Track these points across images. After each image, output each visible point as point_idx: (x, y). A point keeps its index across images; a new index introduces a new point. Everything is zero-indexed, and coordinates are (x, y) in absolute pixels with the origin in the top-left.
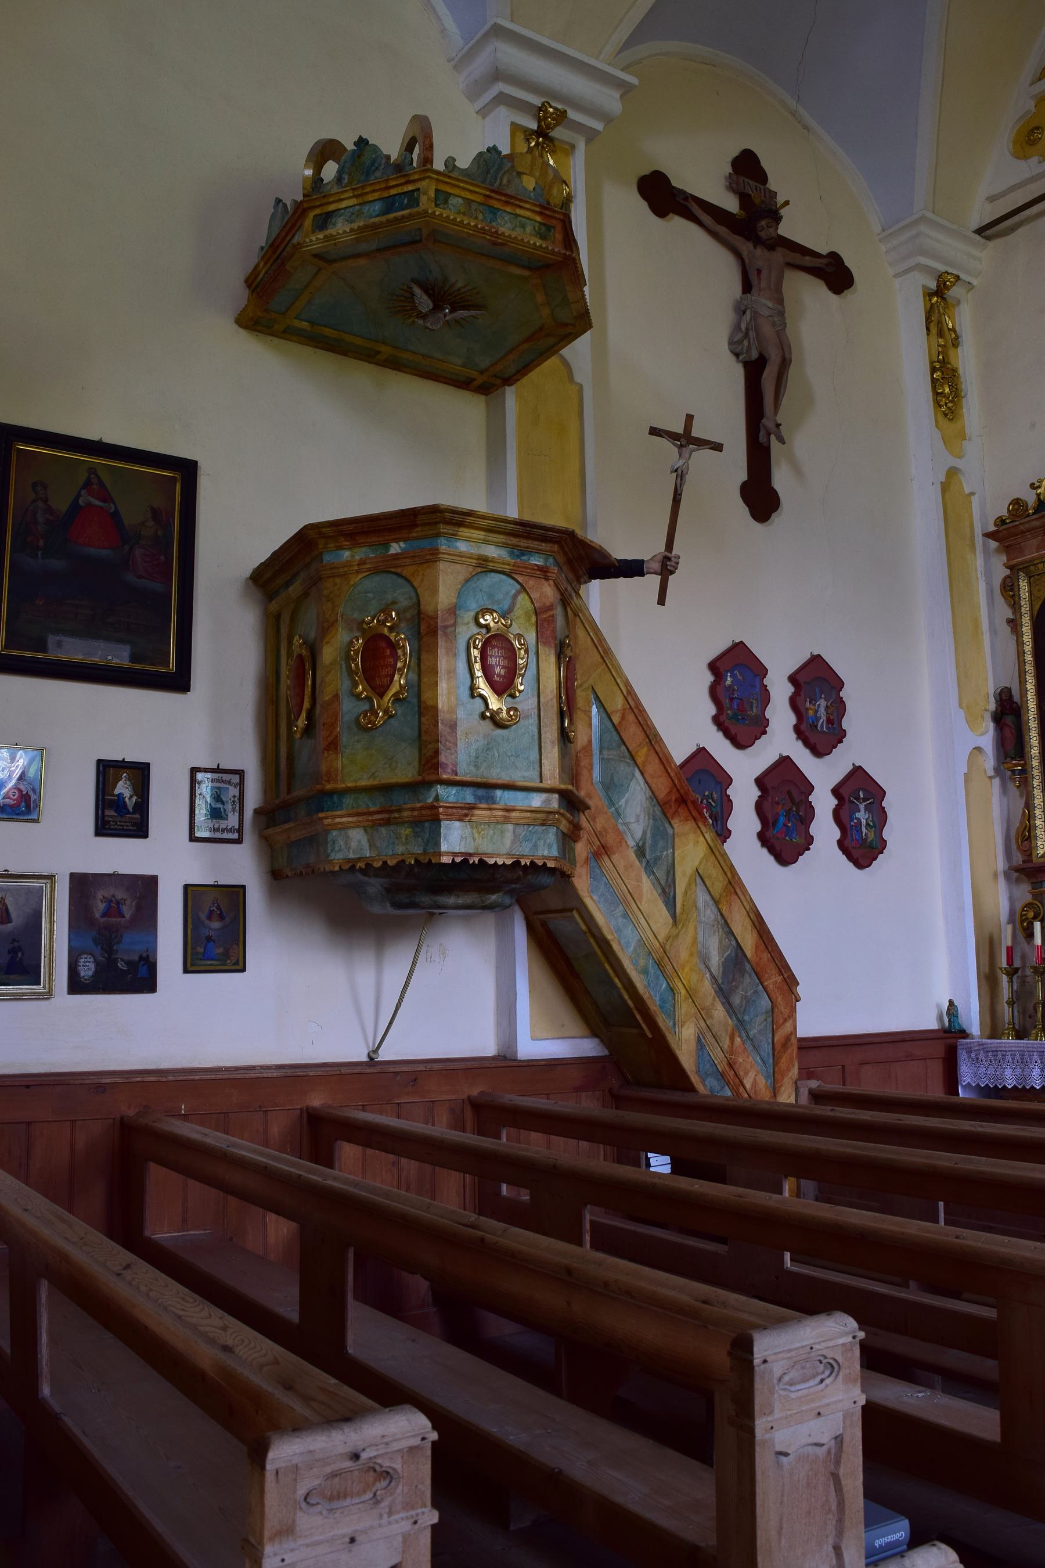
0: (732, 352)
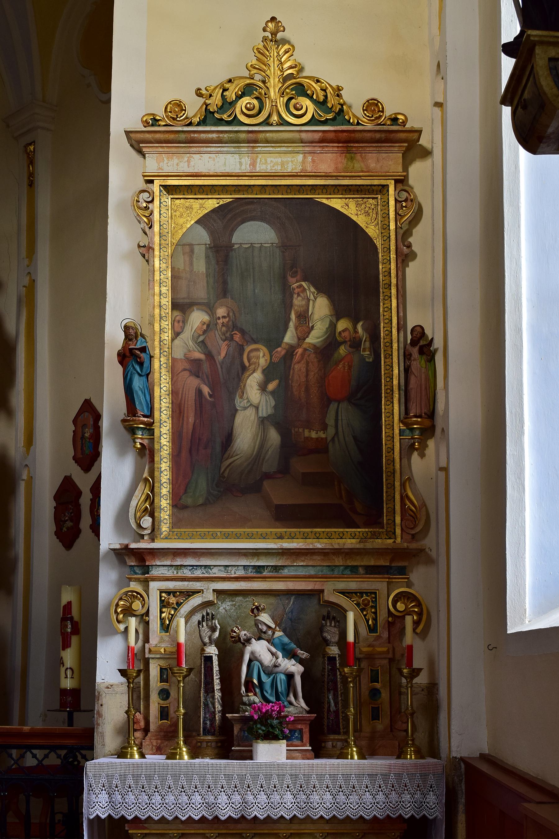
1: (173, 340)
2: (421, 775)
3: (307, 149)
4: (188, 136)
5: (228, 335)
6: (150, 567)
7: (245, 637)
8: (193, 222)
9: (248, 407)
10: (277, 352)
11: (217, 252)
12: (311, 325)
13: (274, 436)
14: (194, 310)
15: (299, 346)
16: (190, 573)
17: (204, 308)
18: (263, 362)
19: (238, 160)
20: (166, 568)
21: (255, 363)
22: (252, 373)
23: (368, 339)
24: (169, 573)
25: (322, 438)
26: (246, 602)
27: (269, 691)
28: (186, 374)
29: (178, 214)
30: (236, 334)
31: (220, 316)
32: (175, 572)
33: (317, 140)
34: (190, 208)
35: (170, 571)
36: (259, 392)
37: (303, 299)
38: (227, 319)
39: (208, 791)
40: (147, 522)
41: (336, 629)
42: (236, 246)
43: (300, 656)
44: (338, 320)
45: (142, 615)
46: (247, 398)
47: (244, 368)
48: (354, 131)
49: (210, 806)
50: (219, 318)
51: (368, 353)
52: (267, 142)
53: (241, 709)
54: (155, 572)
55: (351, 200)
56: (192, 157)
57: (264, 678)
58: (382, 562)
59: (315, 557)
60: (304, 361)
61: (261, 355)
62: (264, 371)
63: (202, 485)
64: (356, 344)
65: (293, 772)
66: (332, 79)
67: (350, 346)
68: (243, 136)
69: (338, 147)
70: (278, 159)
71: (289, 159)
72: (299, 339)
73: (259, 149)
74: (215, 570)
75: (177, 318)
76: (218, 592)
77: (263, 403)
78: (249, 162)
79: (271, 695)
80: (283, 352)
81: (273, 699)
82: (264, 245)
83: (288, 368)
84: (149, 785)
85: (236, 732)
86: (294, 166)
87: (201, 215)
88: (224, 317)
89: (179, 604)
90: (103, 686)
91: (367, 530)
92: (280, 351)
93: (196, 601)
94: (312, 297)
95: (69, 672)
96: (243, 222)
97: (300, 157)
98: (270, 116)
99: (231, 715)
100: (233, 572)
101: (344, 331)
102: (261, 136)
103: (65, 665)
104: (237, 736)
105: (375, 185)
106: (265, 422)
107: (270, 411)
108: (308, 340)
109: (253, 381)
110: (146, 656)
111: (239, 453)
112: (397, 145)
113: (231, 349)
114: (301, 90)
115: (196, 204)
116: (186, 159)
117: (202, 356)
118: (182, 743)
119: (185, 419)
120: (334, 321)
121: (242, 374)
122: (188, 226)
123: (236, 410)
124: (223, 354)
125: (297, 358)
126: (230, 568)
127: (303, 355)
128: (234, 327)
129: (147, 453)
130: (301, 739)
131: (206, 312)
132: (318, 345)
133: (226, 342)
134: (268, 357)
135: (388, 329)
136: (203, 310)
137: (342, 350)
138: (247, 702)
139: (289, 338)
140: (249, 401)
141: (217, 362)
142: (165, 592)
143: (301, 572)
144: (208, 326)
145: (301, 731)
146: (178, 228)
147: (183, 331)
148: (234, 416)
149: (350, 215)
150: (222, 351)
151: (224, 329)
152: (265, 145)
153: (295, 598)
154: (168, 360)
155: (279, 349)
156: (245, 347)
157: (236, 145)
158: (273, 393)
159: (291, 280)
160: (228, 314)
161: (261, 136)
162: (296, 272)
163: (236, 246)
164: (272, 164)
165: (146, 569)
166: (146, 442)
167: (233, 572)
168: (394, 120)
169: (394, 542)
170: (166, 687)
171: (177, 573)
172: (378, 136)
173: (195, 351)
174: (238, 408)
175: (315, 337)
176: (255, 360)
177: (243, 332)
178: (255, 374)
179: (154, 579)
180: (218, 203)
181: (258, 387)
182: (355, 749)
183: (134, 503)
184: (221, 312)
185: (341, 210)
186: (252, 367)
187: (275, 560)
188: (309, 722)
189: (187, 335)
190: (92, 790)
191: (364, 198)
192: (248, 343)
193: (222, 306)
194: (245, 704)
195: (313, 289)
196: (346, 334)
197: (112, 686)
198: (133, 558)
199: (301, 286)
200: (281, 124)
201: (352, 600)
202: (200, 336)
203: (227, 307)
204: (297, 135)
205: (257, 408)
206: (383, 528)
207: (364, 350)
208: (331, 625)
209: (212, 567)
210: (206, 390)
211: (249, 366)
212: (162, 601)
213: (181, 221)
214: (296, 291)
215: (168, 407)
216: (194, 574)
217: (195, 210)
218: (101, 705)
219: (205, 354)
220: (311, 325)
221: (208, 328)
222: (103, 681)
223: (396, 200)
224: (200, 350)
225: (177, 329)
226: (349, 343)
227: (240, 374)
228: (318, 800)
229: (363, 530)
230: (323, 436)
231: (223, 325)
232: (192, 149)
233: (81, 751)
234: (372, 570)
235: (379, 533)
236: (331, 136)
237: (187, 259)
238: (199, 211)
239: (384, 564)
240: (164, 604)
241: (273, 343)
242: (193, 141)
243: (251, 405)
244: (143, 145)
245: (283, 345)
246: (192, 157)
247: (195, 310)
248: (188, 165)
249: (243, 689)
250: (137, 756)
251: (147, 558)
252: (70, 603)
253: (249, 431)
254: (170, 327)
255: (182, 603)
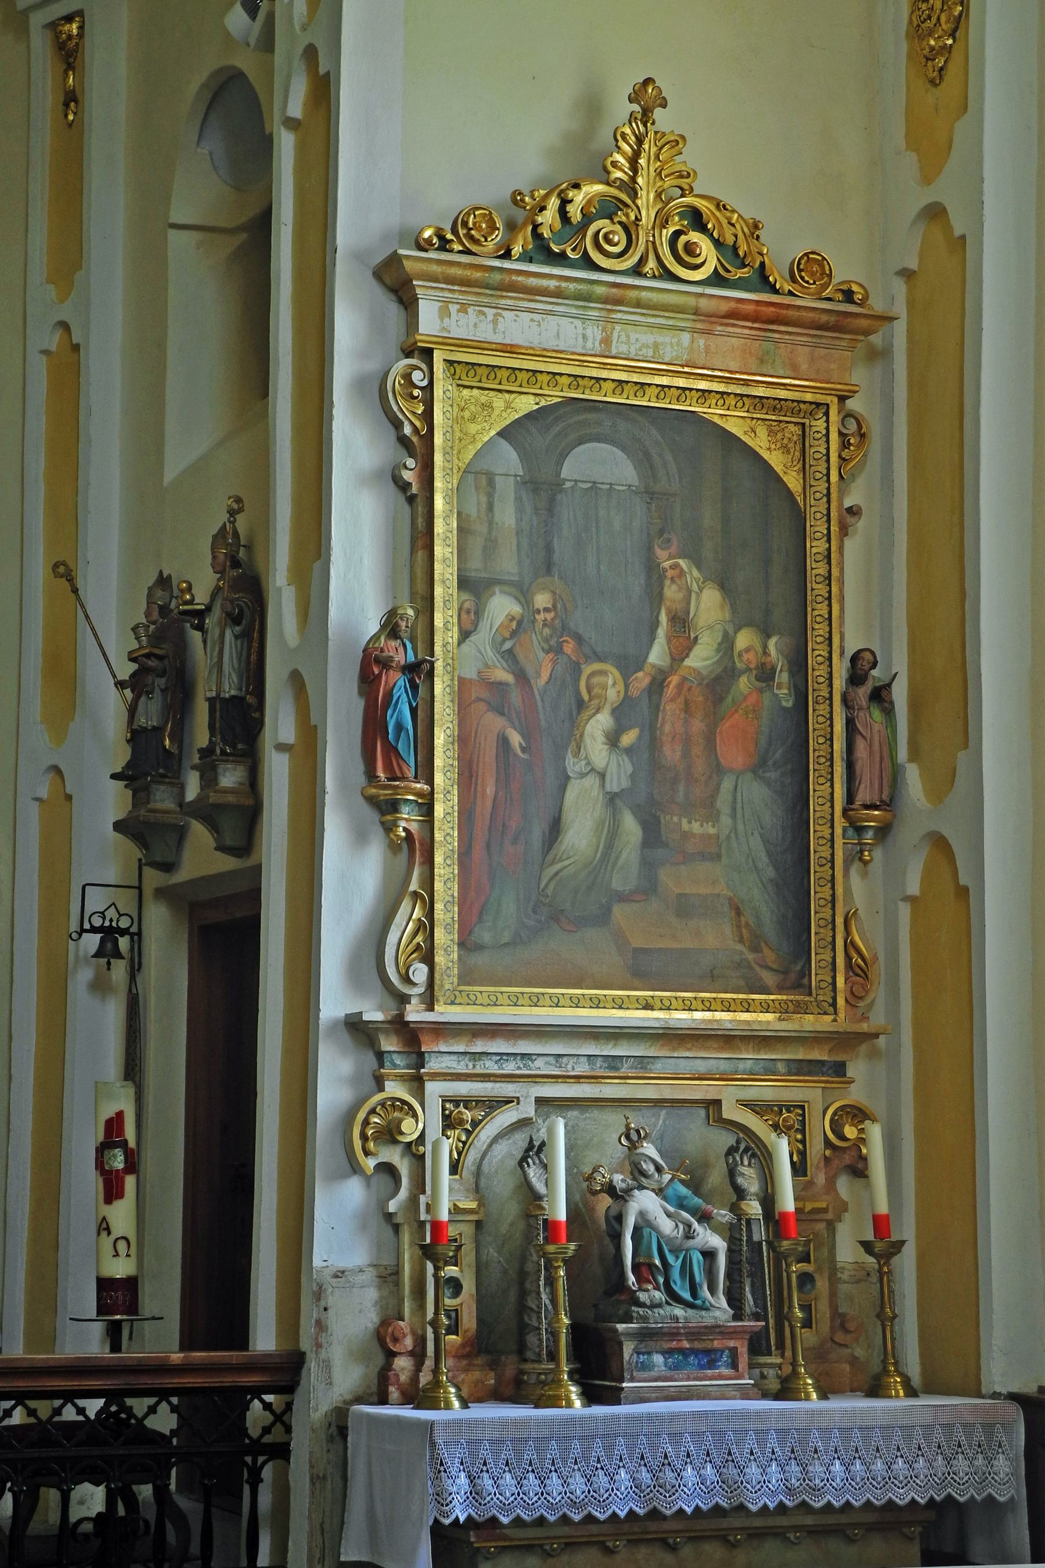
0: (371, 800)
1: (459, 644)
2: (984, 1425)
3: (699, 326)
4: (507, 278)
5: (553, 642)
6: (426, 1055)
7: (624, 1185)
8: (493, 433)
9: (588, 773)
10: (636, 678)
11: (536, 491)
12: (693, 636)
13: (631, 827)
14: (494, 594)
15: (672, 669)
16: (496, 1067)
17: (513, 590)
18: (613, 695)
19: (580, 331)
20: (455, 1057)
21: (598, 696)
22: (594, 714)
23: (786, 668)
24: (461, 1066)
25: (710, 836)
26: (585, 1119)
27: (679, 1282)
28: (482, 706)
29: (467, 414)
30: (567, 641)
31: (541, 608)
32: (471, 1066)
33: (723, 313)
34: (488, 406)
35: (462, 1063)
36: (606, 747)
37: (680, 588)
38: (552, 614)
39: (663, 1465)
40: (420, 973)
41: (752, 1171)
42: (568, 485)
43: (719, 1218)
44: (738, 629)
45: (410, 1144)
46: (586, 758)
47: (581, 705)
48: (789, 307)
49: (642, 1491)
50: (538, 611)
51: (786, 691)
52: (638, 304)
53: (635, 1315)
54: (433, 1065)
55: (759, 422)
56: (500, 315)
57: (671, 1259)
58: (816, 1055)
59: (709, 1043)
60: (681, 700)
61: (610, 683)
62: (614, 711)
63: (509, 907)
64: (766, 675)
65: (780, 1426)
66: (746, 209)
67: (758, 679)
68: (600, 290)
69: (751, 328)
70: (648, 338)
71: (668, 340)
72: (673, 659)
73: (619, 316)
74: (539, 1062)
75: (467, 605)
76: (540, 1101)
77: (613, 766)
78: (599, 337)
79: (682, 1288)
80: (647, 681)
81: (686, 1295)
82: (617, 487)
83: (655, 709)
84: (610, 1458)
85: (626, 1356)
86: (675, 353)
87: (508, 422)
88: (546, 610)
89: (475, 1124)
90: (327, 1273)
91: (785, 997)
92: (642, 679)
93: (506, 1117)
94: (695, 587)
95: (122, 1246)
96: (581, 442)
97: (686, 337)
98: (642, 261)
99: (624, 1325)
100: (569, 1067)
101: (747, 650)
102: (632, 294)
103: (112, 1229)
104: (629, 1363)
105: (805, 402)
106: (619, 803)
107: (625, 783)
108: (688, 662)
109: (598, 724)
110: (422, 1219)
111: (571, 854)
112: (848, 336)
113: (559, 668)
114: (697, 220)
115: (499, 402)
116: (490, 318)
117: (509, 678)
118: (566, 1377)
119: (479, 788)
120: (731, 631)
121: (579, 713)
122: (486, 439)
123: (568, 778)
124: (545, 676)
125: (670, 691)
126: (565, 1059)
127: (680, 686)
128: (563, 629)
129: (419, 849)
130: (734, 1366)
131: (516, 598)
132: (704, 672)
133: (551, 655)
134: (621, 687)
135: (823, 653)
136: (509, 594)
137: (744, 683)
138: (648, 1303)
139: (657, 655)
140: (588, 764)
141: (536, 691)
142: (450, 1101)
143: (701, 1066)
144: (520, 623)
145: (734, 1352)
146: (468, 441)
147: (475, 630)
148: (563, 788)
149: (757, 449)
150: (543, 670)
151: (547, 631)
152: (632, 310)
153: (667, 1114)
154: (452, 680)
155: (640, 674)
156: (583, 666)
157: (581, 303)
158: (629, 751)
159: (661, 554)
160: (554, 606)
161: (632, 294)
162: (669, 541)
163: (568, 485)
164: (638, 345)
165: (420, 1060)
166: (414, 827)
167: (569, 1067)
168: (848, 296)
169: (835, 1020)
170: (454, 1275)
171: (474, 1066)
172: (824, 318)
173: (496, 667)
174: (571, 775)
175: (701, 658)
176: (600, 691)
177: (579, 640)
178: (599, 716)
179: (436, 1076)
180: (537, 404)
181: (603, 739)
182: (809, 1381)
183: (392, 938)
184: (542, 600)
185: (744, 438)
186: (595, 703)
187: (642, 1047)
188: (747, 1337)
189: (483, 637)
190: (445, 1471)
191: (781, 421)
192: (588, 659)
193: (543, 589)
194: (642, 1305)
195: (696, 573)
196: (750, 656)
197: (343, 1272)
198: (394, 1039)
199: (675, 566)
200: (660, 277)
201: (765, 1118)
202: (505, 640)
203: (554, 593)
204: (692, 301)
205: (602, 776)
206: (810, 994)
207: (779, 687)
208: (750, 1165)
209: (534, 1057)
210: (516, 739)
211: (590, 700)
212: (446, 1118)
213: (473, 428)
214: (670, 573)
215: (452, 765)
216: (503, 1069)
217: (497, 412)
218: (326, 1309)
219: (513, 673)
220: (693, 636)
221: (518, 628)
222: (325, 1264)
223: (840, 433)
224: (505, 665)
225: (468, 626)
226: (754, 672)
227: (574, 713)
228: (823, 1475)
229: (779, 997)
230: (712, 831)
231: (545, 625)
232: (504, 302)
233: (263, 1396)
234: (802, 1069)
235: (806, 1003)
236: (750, 308)
237: (484, 499)
238: (504, 414)
239: (819, 1058)
240: (449, 1122)
241: (629, 665)
242: (513, 287)
243: (593, 769)
244: (420, 283)
245: (647, 668)
246: (500, 315)
247: (498, 592)
248: (494, 329)
249: (631, 1278)
250: (456, 1404)
251: (424, 1038)
252: (120, 1115)
253: (588, 815)
254: (456, 620)
255: (481, 1121)
